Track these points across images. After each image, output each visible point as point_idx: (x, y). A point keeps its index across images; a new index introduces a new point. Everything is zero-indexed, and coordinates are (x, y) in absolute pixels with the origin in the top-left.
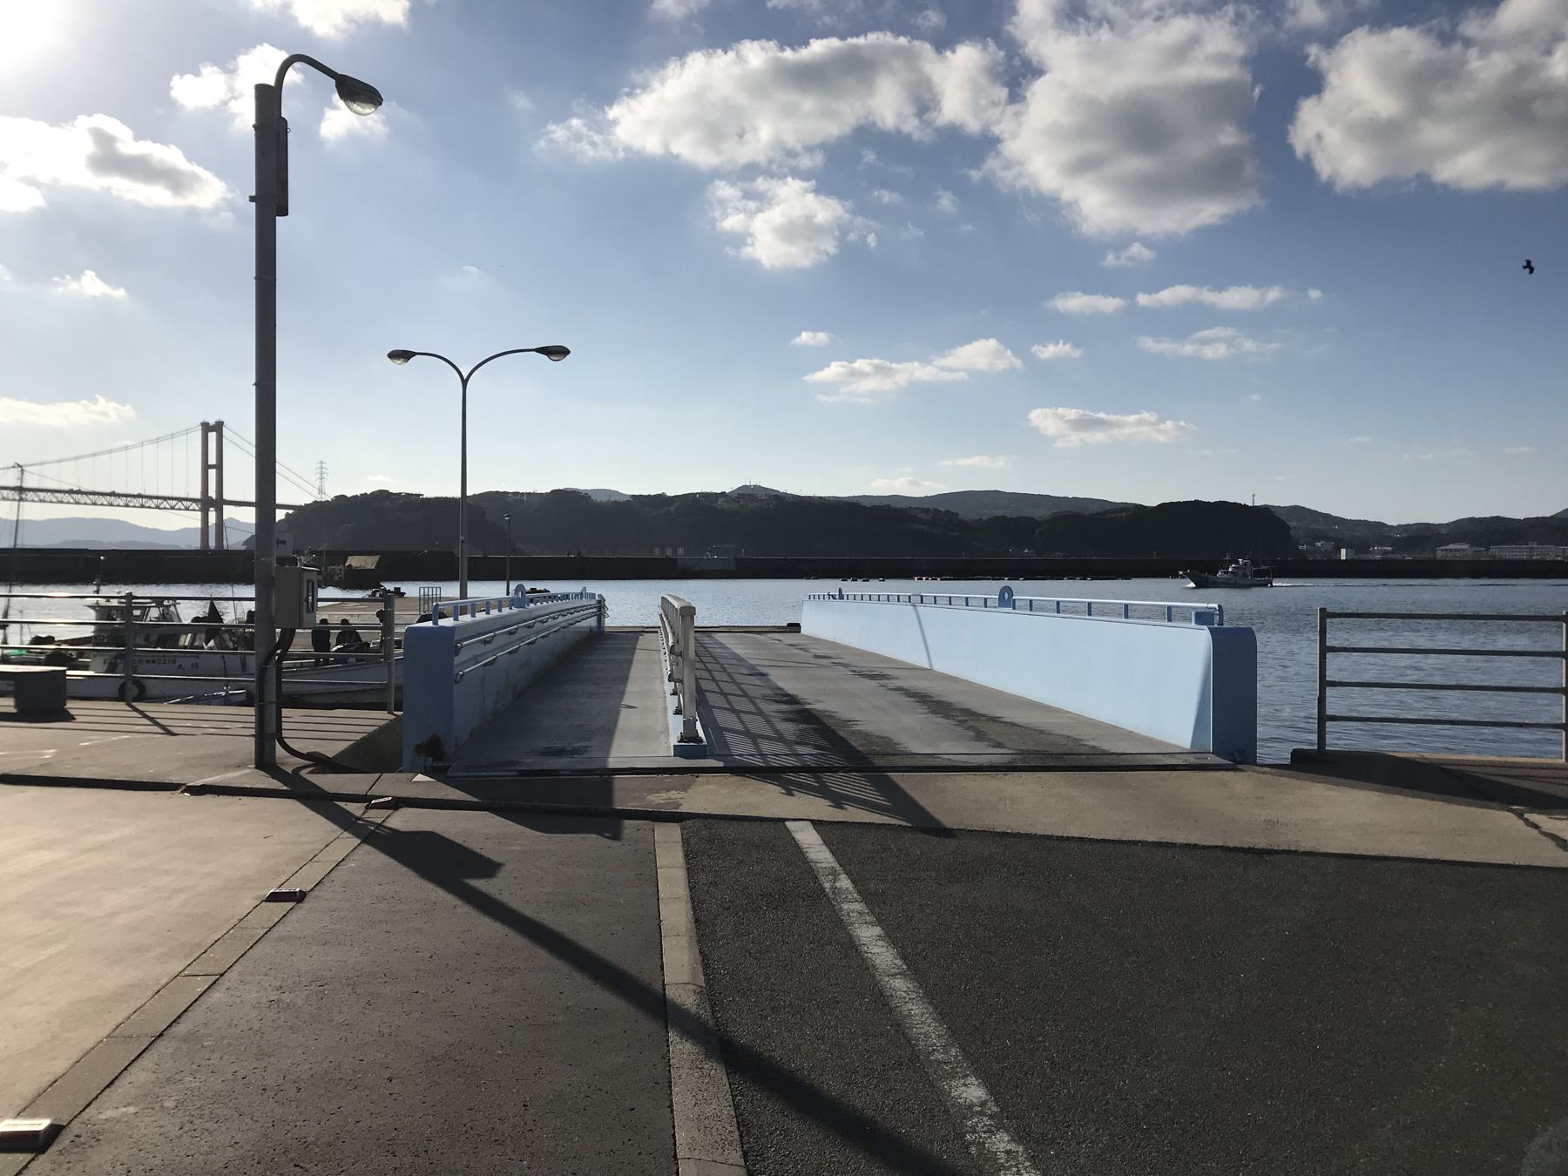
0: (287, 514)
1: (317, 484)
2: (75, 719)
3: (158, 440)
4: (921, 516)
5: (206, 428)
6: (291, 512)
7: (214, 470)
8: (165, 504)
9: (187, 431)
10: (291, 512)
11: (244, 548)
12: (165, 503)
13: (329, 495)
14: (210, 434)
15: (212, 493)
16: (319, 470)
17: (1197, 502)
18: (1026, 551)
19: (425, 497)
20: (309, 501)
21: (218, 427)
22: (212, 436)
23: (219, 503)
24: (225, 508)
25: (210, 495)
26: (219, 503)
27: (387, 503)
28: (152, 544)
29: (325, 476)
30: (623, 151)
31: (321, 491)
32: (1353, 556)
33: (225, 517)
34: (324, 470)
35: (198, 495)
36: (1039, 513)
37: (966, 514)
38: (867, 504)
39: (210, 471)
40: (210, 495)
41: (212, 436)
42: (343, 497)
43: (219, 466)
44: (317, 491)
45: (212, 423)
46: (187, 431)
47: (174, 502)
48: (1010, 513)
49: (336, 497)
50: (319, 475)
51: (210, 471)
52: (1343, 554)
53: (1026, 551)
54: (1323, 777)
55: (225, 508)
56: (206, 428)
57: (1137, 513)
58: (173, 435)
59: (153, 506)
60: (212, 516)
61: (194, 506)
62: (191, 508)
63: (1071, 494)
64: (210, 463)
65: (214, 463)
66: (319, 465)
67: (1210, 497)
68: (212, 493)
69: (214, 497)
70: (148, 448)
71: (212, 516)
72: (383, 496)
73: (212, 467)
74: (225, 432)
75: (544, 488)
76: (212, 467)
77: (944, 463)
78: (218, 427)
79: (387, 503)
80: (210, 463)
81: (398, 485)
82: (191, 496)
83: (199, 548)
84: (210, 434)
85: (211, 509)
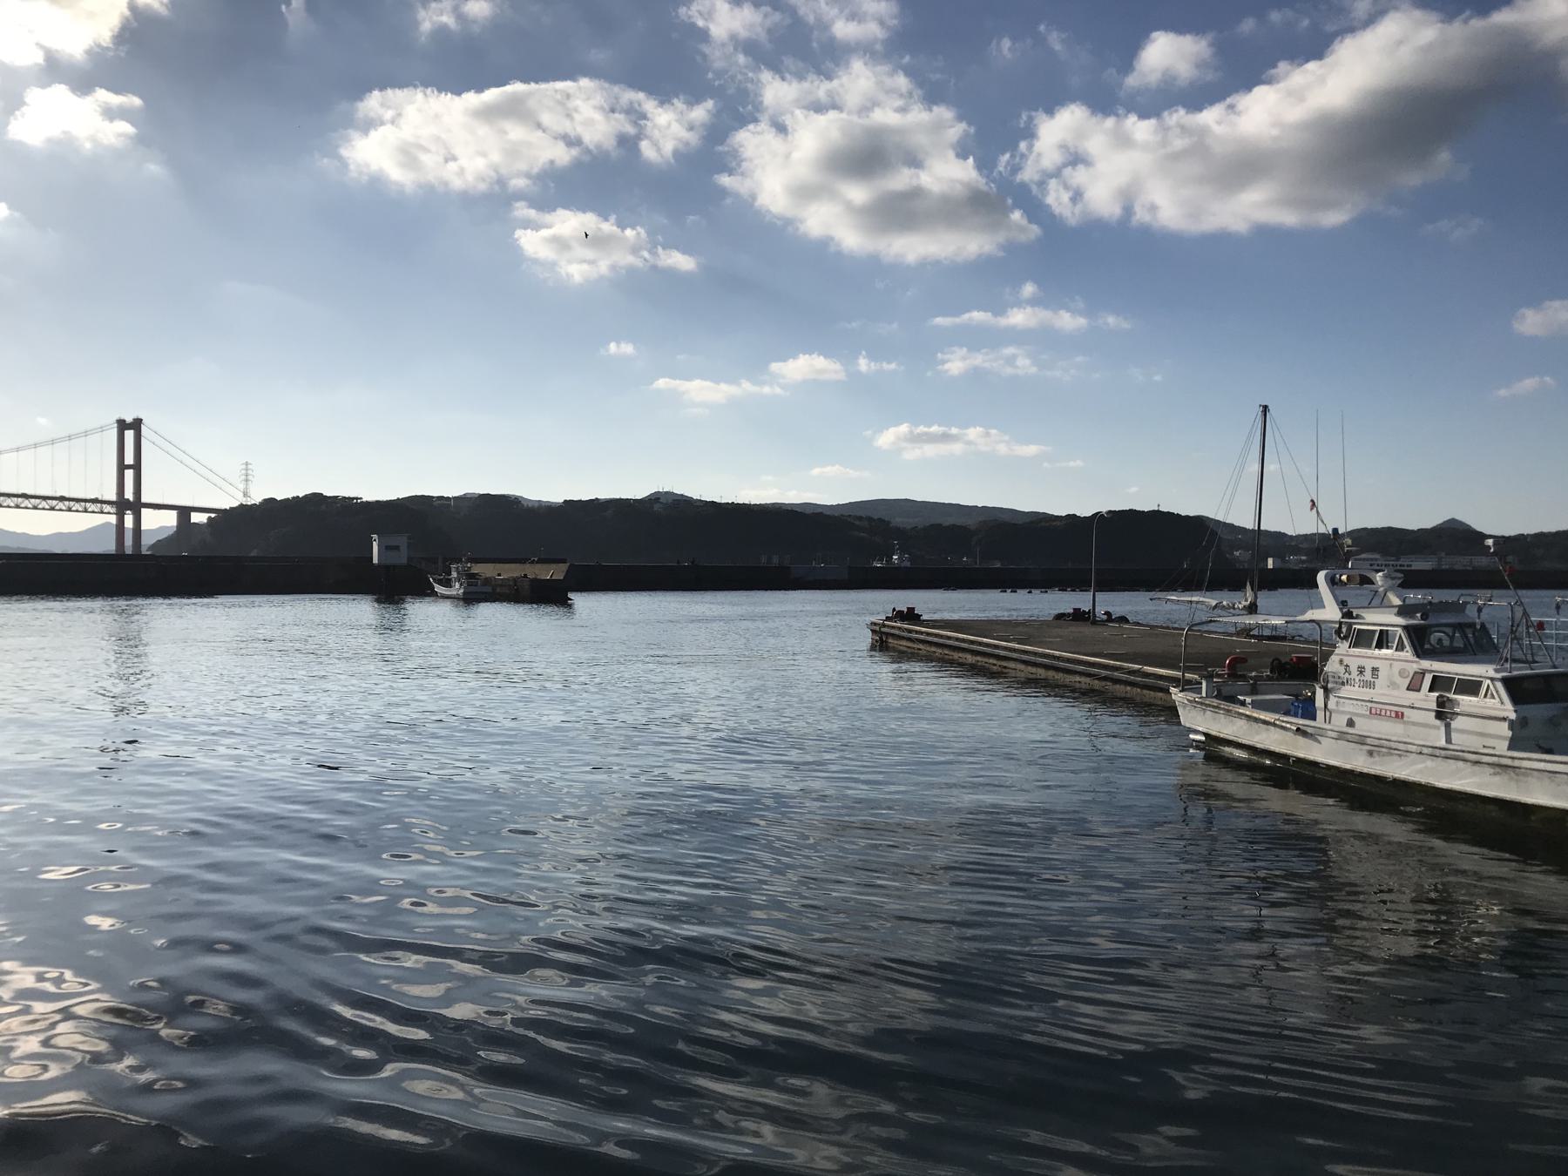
0: (209, 518)
1: (242, 486)
2: (231, 1007)
3: (53, 442)
4: (857, 523)
5: (122, 426)
6: (213, 515)
7: (131, 471)
8: (26, 503)
9: (102, 429)
10: (213, 515)
11: (149, 553)
12: (26, 502)
13: (256, 498)
14: (126, 432)
15: (129, 494)
16: (244, 472)
17: (1131, 511)
18: (965, 559)
19: (364, 500)
20: (235, 504)
21: (137, 425)
22: (129, 435)
23: (137, 506)
24: (144, 511)
25: (126, 497)
26: (137, 506)
27: (324, 507)
28: (24, 549)
29: (250, 477)
30: (720, 85)
31: (245, 494)
32: (1279, 564)
33: (143, 527)
34: (250, 472)
35: (113, 498)
36: (971, 522)
37: (898, 521)
38: (808, 511)
39: (126, 471)
40: (126, 497)
41: (129, 435)
42: (271, 501)
43: (137, 467)
44: (242, 494)
45: (129, 419)
46: (102, 429)
47: (38, 501)
48: (948, 521)
49: (265, 500)
50: (244, 477)
51: (126, 471)
52: (1270, 563)
53: (965, 559)
54: (58, 549)
55: (144, 511)
56: (122, 426)
57: (1072, 522)
58: (70, 438)
59: (12, 504)
60: (129, 520)
61: (107, 508)
62: (57, 508)
63: (980, 502)
64: (126, 463)
65: (132, 462)
66: (244, 467)
67: (604, 495)
68: (129, 494)
69: (131, 499)
70: (44, 451)
71: (129, 520)
72: (316, 499)
73: (129, 467)
74: (143, 428)
75: (558, 498)
76: (129, 467)
77: (816, 471)
78: (137, 425)
79: (324, 507)
80: (126, 463)
81: (332, 488)
82: (106, 498)
83: (114, 552)
84: (126, 432)
85: (128, 512)
